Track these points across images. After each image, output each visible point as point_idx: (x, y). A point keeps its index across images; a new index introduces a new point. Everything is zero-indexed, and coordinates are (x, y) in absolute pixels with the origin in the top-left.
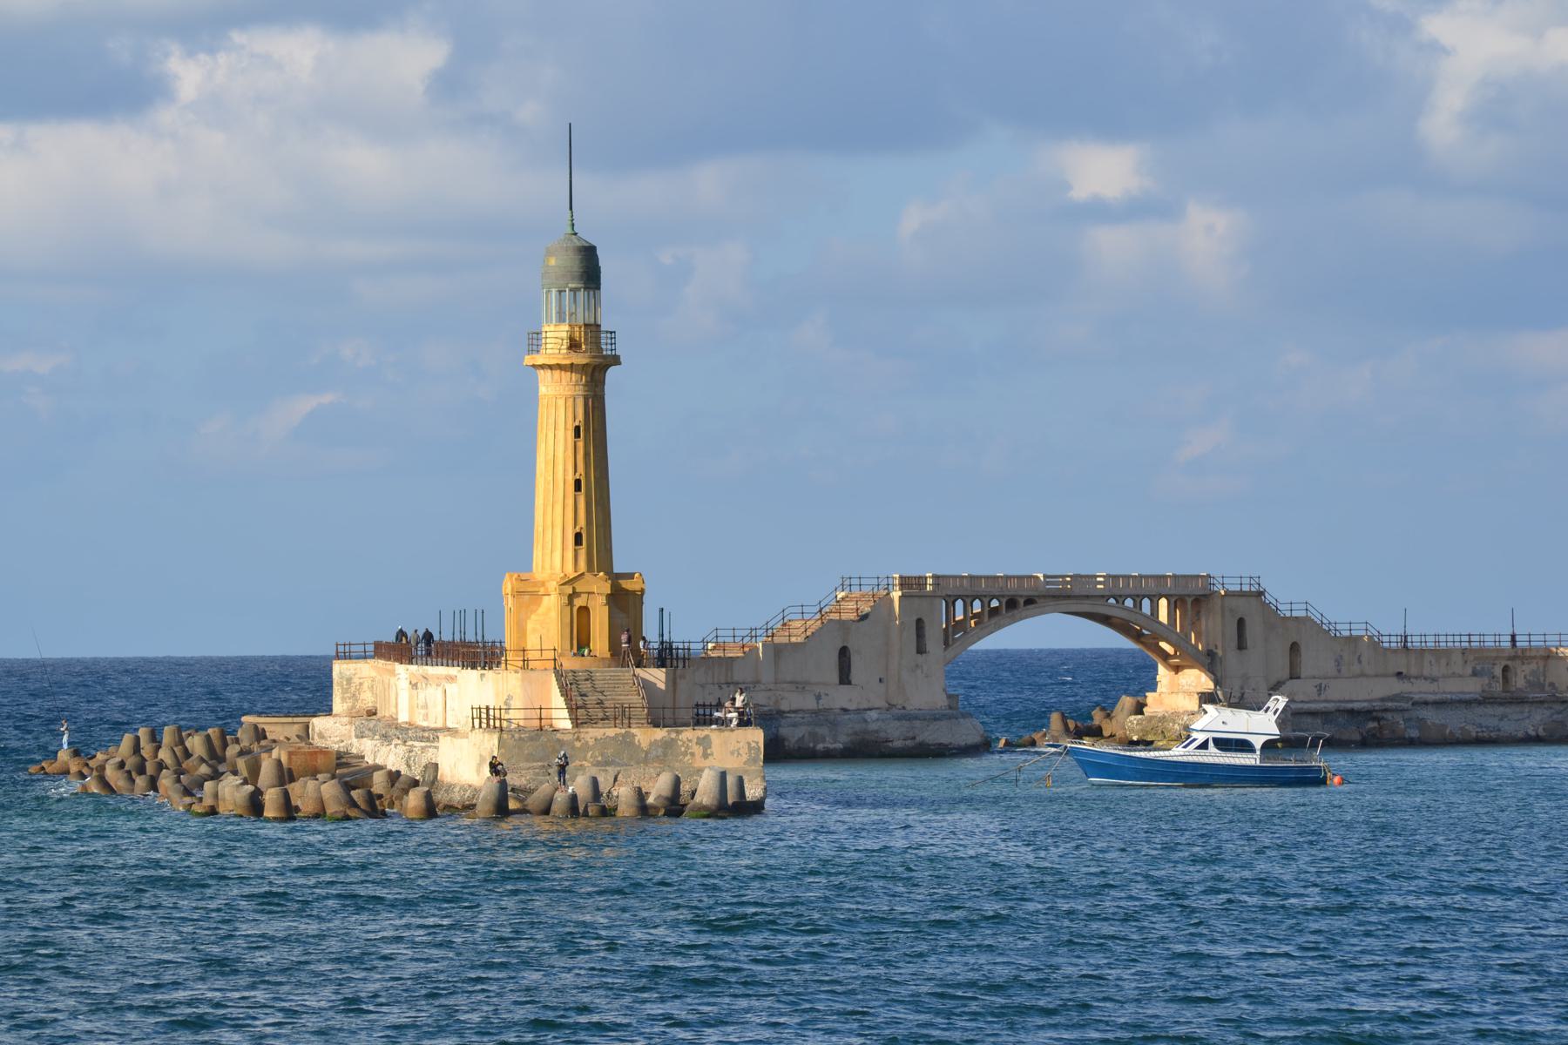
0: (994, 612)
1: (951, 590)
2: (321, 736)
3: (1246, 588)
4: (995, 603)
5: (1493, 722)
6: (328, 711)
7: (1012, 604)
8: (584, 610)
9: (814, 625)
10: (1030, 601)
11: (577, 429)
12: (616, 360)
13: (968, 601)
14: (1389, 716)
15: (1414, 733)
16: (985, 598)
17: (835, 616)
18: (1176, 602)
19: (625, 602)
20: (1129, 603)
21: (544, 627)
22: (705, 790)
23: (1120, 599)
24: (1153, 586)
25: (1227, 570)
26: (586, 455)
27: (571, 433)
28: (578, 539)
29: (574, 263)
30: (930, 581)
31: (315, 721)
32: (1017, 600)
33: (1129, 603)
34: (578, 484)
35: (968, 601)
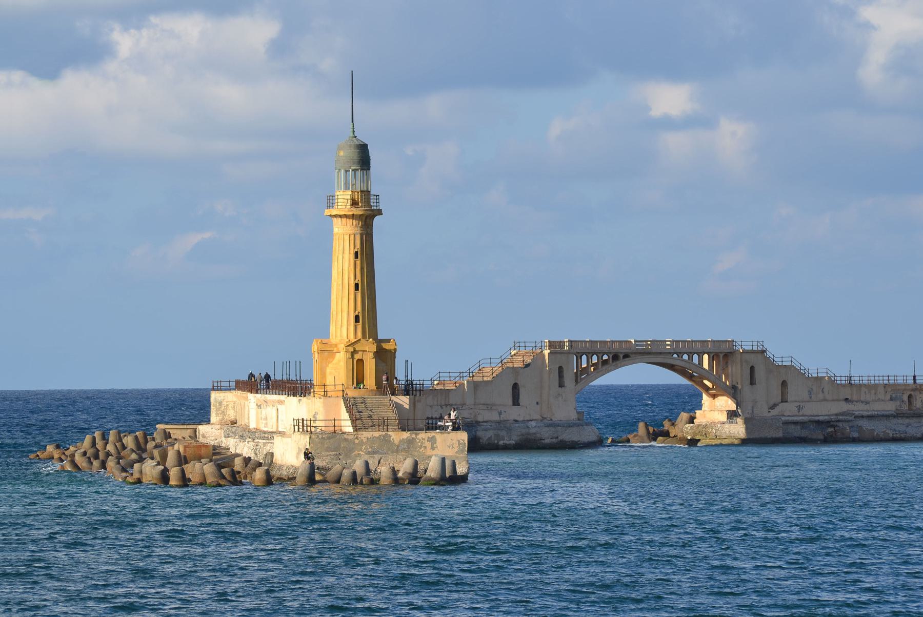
0: (605, 362)
1: (579, 349)
2: (204, 436)
3: (755, 348)
4: (605, 357)
5: (902, 428)
6: (208, 422)
7: (615, 357)
8: (361, 361)
9: (498, 370)
10: (626, 356)
11: (356, 253)
12: (379, 212)
13: (589, 356)
14: (840, 424)
15: (855, 435)
16: (599, 354)
17: (510, 365)
18: (713, 357)
19: (385, 357)
20: (685, 357)
21: (336, 371)
22: (432, 469)
23: (680, 354)
24: (700, 348)
25: (744, 337)
26: (362, 269)
27: (353, 256)
28: (357, 319)
29: (354, 154)
30: (567, 344)
31: (200, 427)
32: (618, 355)
33: (685, 357)
34: (357, 286)
35: (589, 356)
